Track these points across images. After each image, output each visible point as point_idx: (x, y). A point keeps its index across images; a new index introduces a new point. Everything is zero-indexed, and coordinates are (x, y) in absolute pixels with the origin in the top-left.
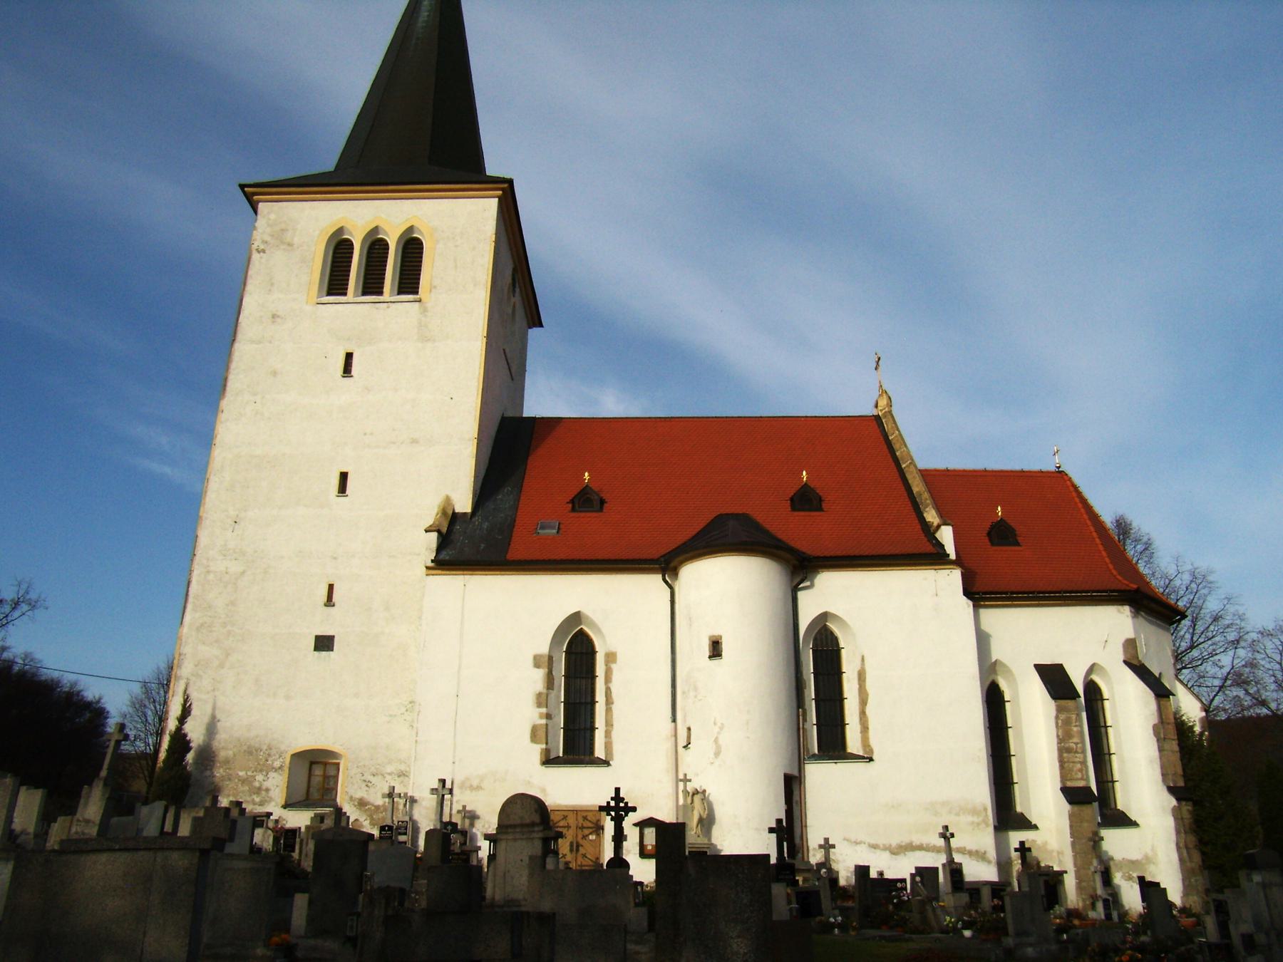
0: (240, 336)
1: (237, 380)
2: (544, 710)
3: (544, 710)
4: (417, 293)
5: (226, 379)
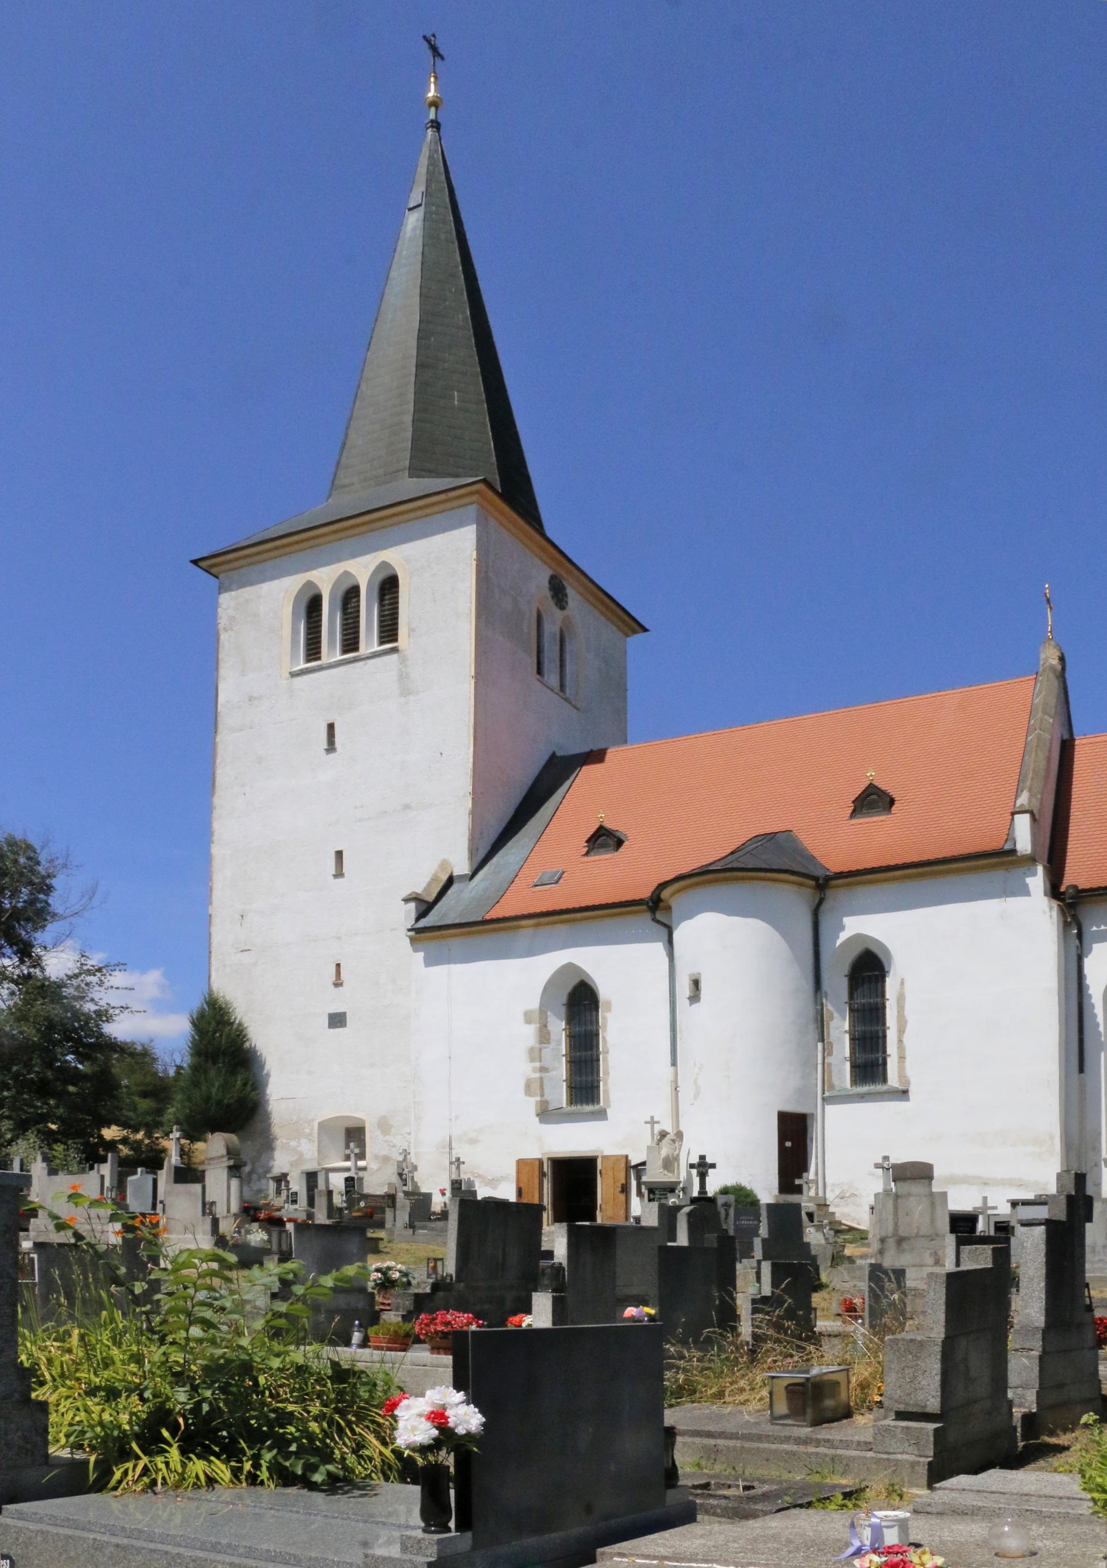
0: (221, 727)
1: (224, 774)
2: (537, 1064)
3: (537, 1064)
4: (396, 640)
5: (214, 774)
